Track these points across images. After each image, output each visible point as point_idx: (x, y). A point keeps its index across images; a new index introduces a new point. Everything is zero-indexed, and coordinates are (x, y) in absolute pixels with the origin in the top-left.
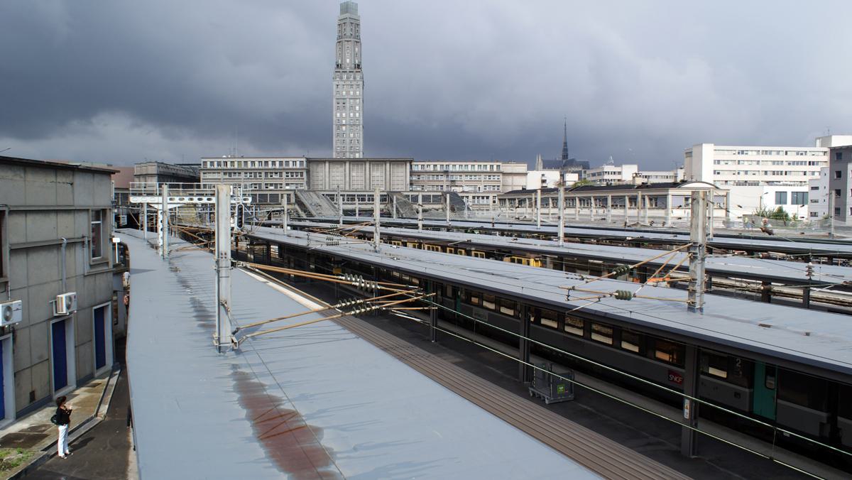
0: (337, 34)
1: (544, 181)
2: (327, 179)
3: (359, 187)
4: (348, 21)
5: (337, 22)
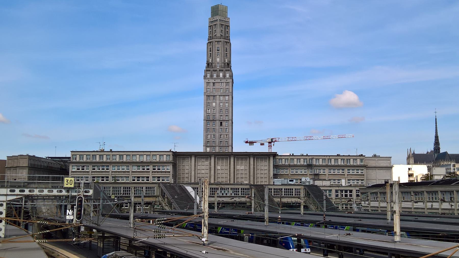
1: (410, 175)
2: (193, 173)
3: (224, 180)
5: (207, 25)
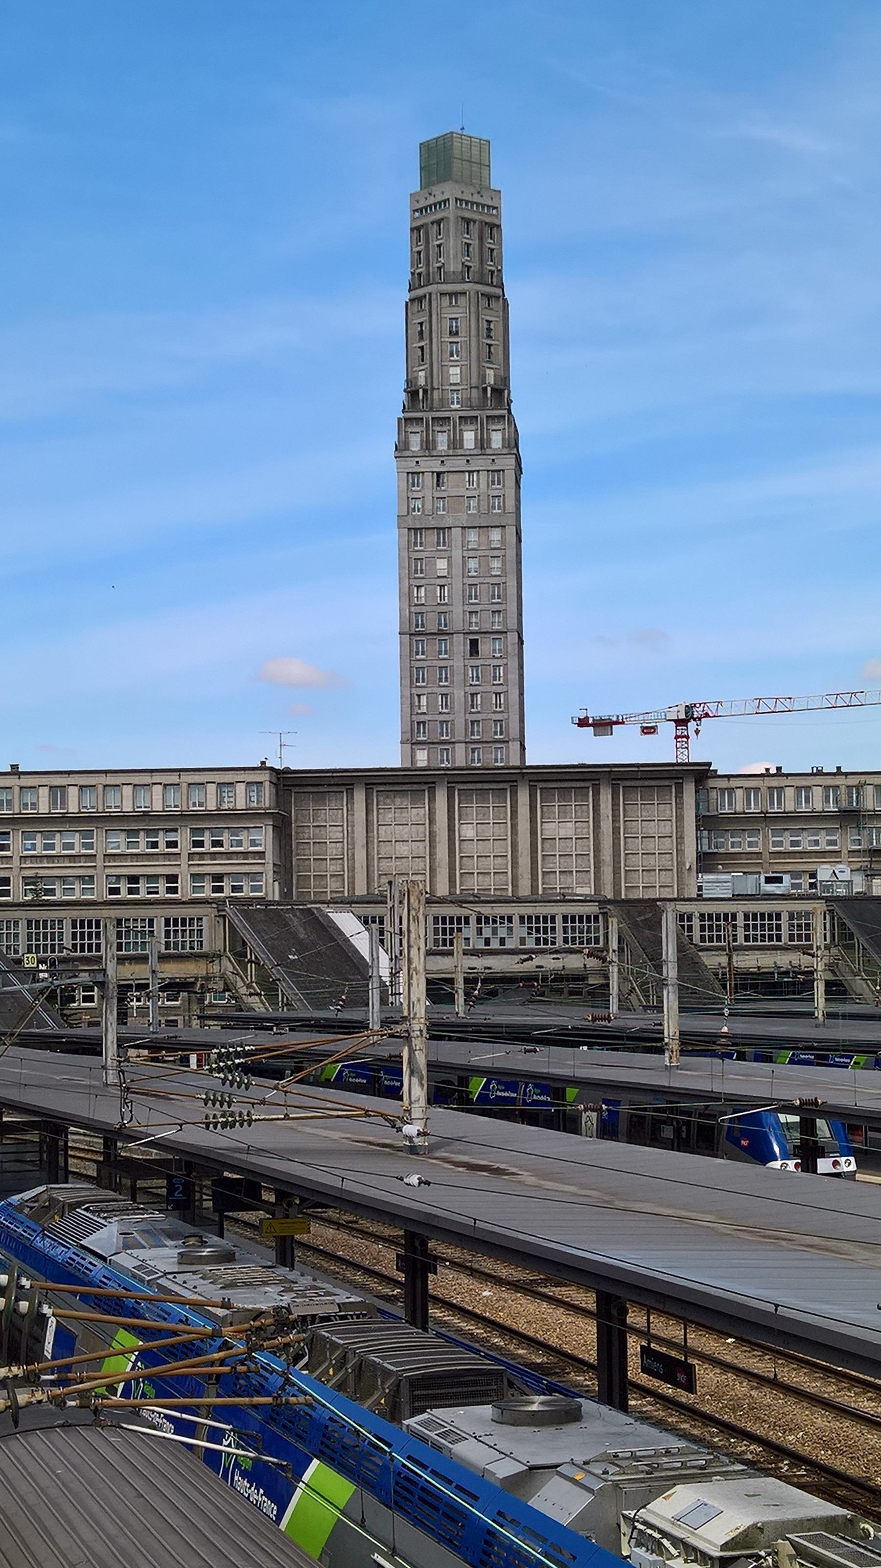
0: (409, 270)
3: (490, 882)
4: (451, 212)
